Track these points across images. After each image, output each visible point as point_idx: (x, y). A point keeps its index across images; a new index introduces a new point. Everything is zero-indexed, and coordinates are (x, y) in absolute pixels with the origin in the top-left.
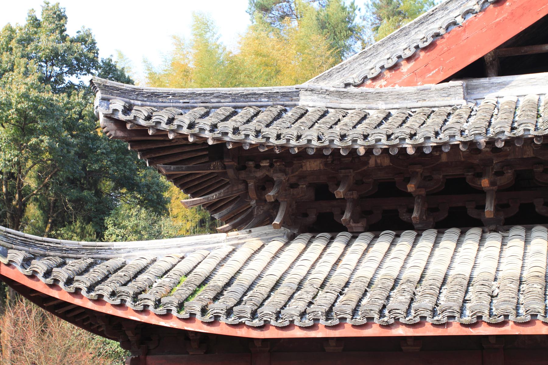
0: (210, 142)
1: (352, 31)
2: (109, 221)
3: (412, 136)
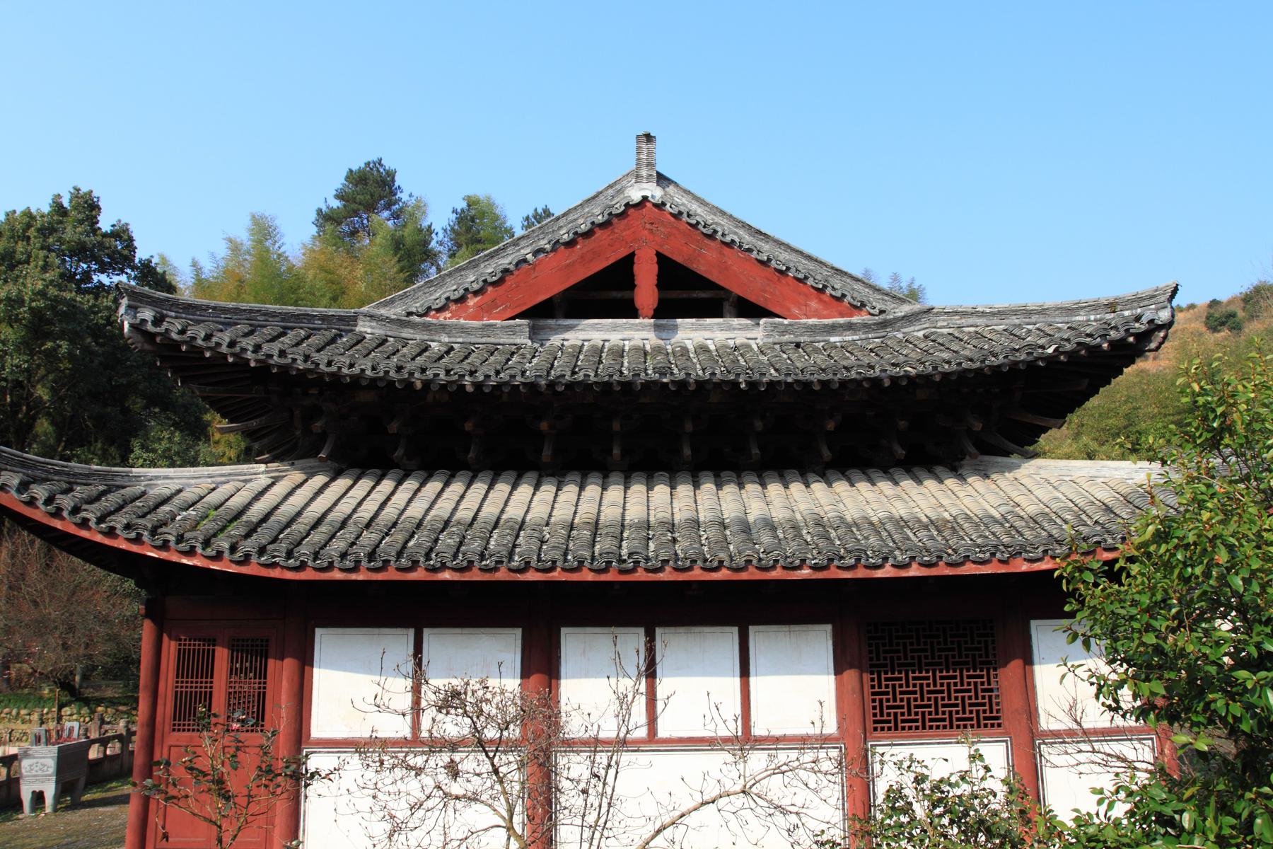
0: (253, 364)
1: (430, 256)
2: (136, 444)
3: (472, 373)
